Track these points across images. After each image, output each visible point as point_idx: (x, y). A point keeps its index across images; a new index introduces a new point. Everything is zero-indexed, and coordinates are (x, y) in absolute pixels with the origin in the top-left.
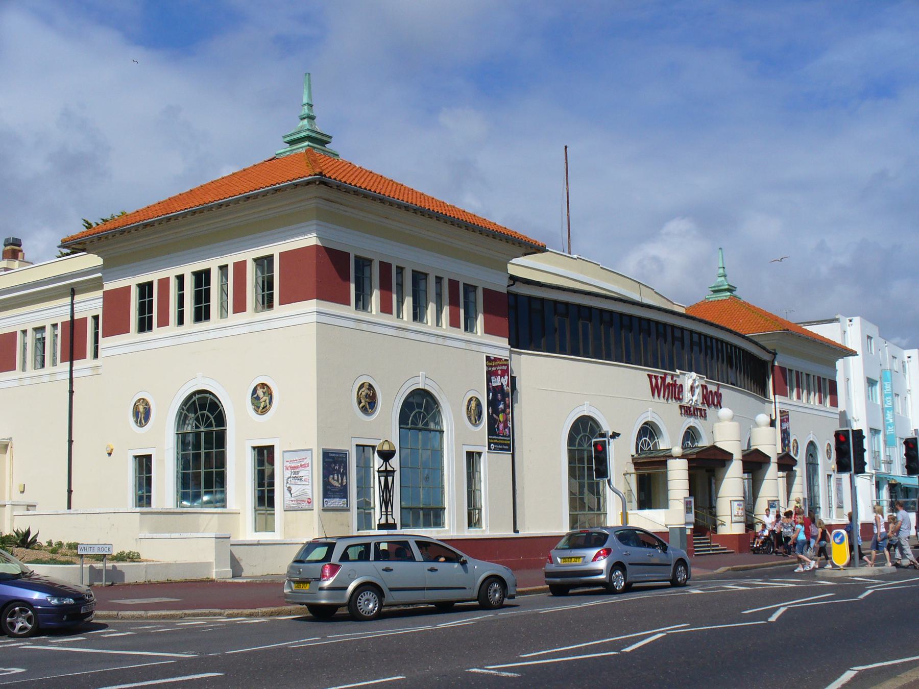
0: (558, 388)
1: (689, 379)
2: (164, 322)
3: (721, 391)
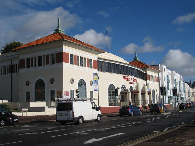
1: (130, 77)
2: (32, 66)
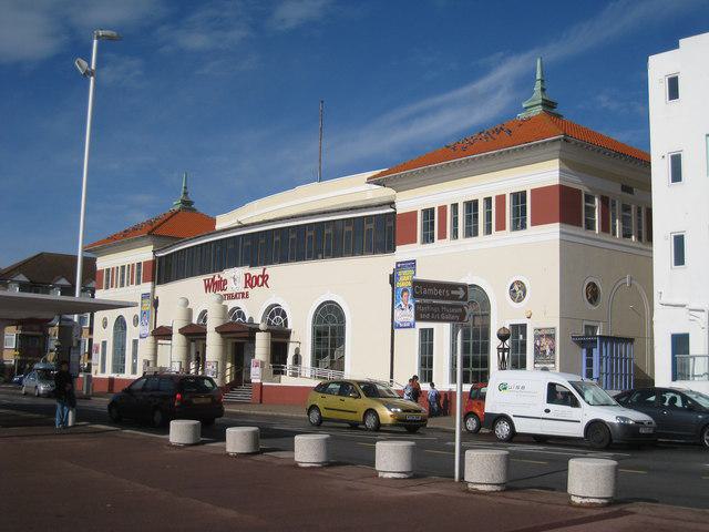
1: (227, 274)
2: (442, 236)
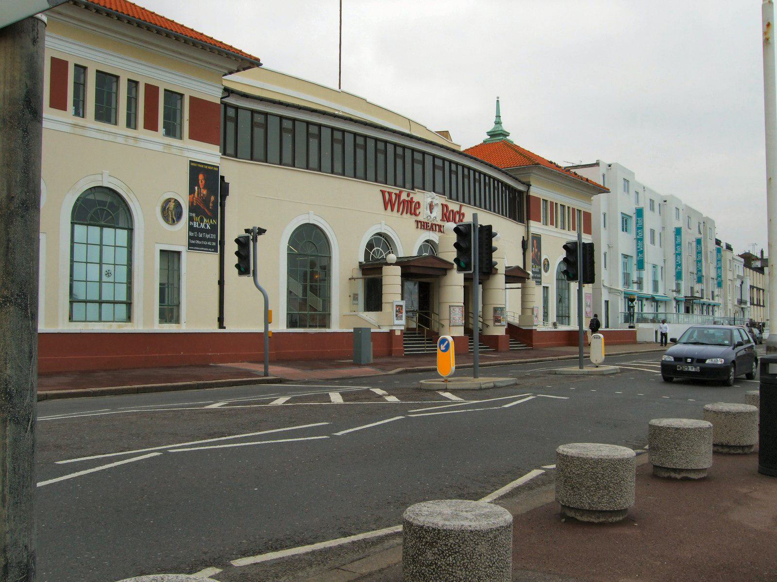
0: (270, 199)
1: (423, 198)
3: (464, 210)
